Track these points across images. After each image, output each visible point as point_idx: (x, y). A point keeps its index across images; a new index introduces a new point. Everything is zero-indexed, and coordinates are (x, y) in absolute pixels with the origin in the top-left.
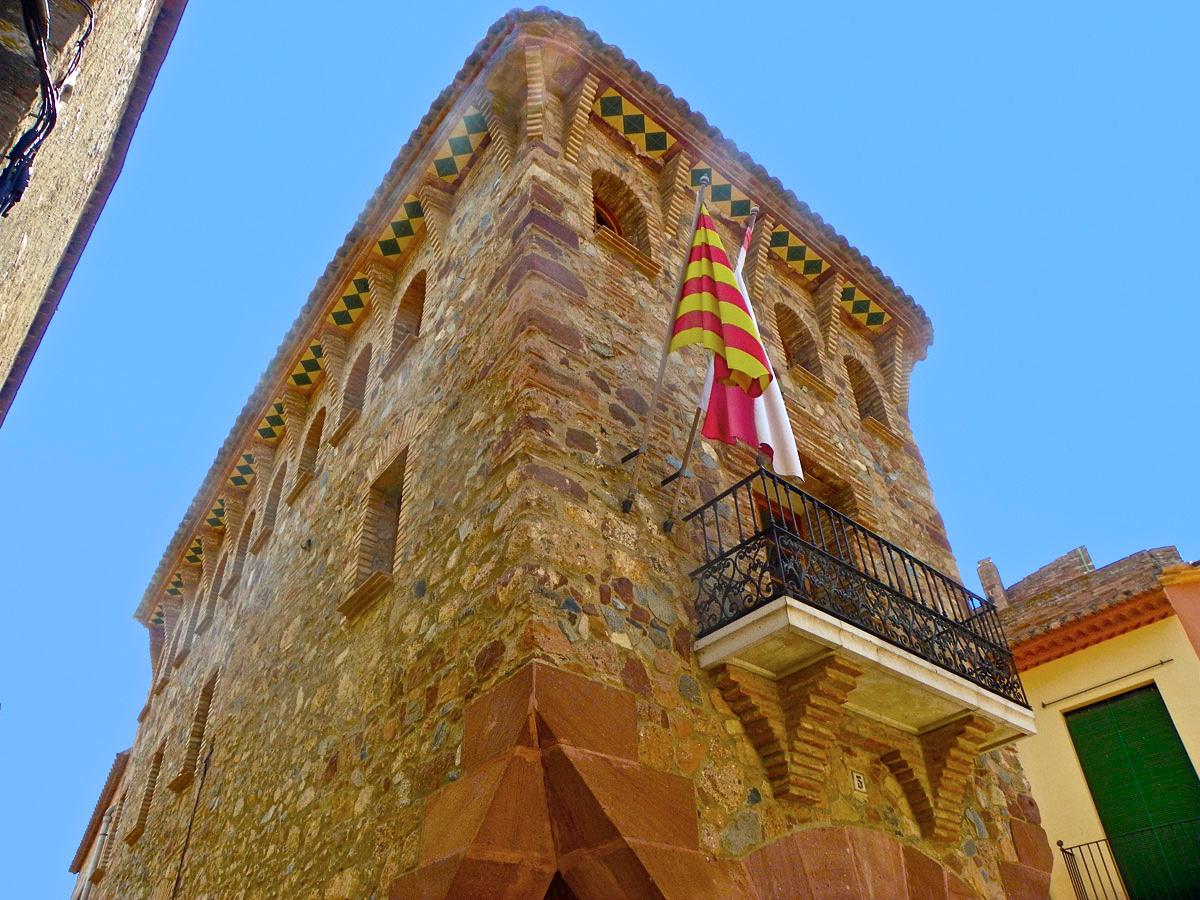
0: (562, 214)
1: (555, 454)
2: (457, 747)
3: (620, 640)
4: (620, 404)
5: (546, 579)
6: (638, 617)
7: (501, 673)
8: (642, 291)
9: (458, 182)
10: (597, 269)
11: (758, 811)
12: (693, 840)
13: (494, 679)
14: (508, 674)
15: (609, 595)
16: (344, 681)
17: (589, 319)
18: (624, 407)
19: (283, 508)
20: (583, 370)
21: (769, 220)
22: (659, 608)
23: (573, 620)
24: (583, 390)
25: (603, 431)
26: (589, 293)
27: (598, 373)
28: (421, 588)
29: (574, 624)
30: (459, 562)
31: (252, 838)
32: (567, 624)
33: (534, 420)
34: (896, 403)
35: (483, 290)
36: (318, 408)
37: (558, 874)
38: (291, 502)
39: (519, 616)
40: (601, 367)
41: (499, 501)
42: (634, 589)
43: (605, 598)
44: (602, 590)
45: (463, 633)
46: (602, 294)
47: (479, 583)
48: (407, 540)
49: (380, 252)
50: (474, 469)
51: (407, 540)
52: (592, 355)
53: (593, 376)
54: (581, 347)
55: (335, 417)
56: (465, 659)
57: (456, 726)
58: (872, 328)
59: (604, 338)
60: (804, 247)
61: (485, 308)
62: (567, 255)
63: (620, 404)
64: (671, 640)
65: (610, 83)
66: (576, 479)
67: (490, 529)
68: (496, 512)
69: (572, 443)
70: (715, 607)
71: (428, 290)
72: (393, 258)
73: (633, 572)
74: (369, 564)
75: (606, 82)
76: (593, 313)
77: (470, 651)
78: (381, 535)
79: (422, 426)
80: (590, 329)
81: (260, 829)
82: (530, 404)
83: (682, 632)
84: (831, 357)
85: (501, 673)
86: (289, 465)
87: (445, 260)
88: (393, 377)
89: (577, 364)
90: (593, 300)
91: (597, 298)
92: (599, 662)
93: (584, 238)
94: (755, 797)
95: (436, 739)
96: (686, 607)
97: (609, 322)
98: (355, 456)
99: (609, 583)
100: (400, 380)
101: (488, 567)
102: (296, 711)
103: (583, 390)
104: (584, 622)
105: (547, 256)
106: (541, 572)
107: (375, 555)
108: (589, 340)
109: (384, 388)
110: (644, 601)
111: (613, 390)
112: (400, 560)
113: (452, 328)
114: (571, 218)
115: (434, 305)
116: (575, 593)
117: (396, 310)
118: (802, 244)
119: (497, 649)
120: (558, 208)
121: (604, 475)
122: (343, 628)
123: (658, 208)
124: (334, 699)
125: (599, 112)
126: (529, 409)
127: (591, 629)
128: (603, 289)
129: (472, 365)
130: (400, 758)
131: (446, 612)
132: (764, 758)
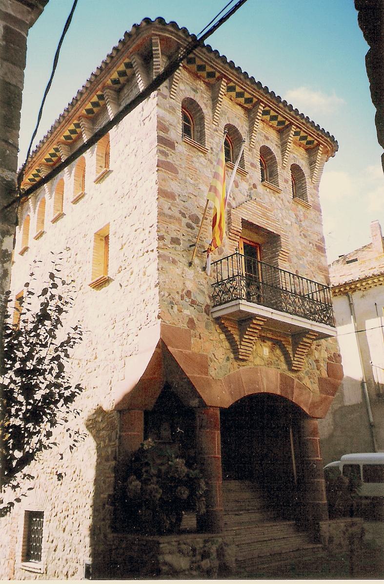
3: (187, 312)
17: (179, 185)
18: (191, 223)
76: (181, 181)
84: (283, 168)
89: (175, 208)
94: (228, 359)
110: (195, 297)
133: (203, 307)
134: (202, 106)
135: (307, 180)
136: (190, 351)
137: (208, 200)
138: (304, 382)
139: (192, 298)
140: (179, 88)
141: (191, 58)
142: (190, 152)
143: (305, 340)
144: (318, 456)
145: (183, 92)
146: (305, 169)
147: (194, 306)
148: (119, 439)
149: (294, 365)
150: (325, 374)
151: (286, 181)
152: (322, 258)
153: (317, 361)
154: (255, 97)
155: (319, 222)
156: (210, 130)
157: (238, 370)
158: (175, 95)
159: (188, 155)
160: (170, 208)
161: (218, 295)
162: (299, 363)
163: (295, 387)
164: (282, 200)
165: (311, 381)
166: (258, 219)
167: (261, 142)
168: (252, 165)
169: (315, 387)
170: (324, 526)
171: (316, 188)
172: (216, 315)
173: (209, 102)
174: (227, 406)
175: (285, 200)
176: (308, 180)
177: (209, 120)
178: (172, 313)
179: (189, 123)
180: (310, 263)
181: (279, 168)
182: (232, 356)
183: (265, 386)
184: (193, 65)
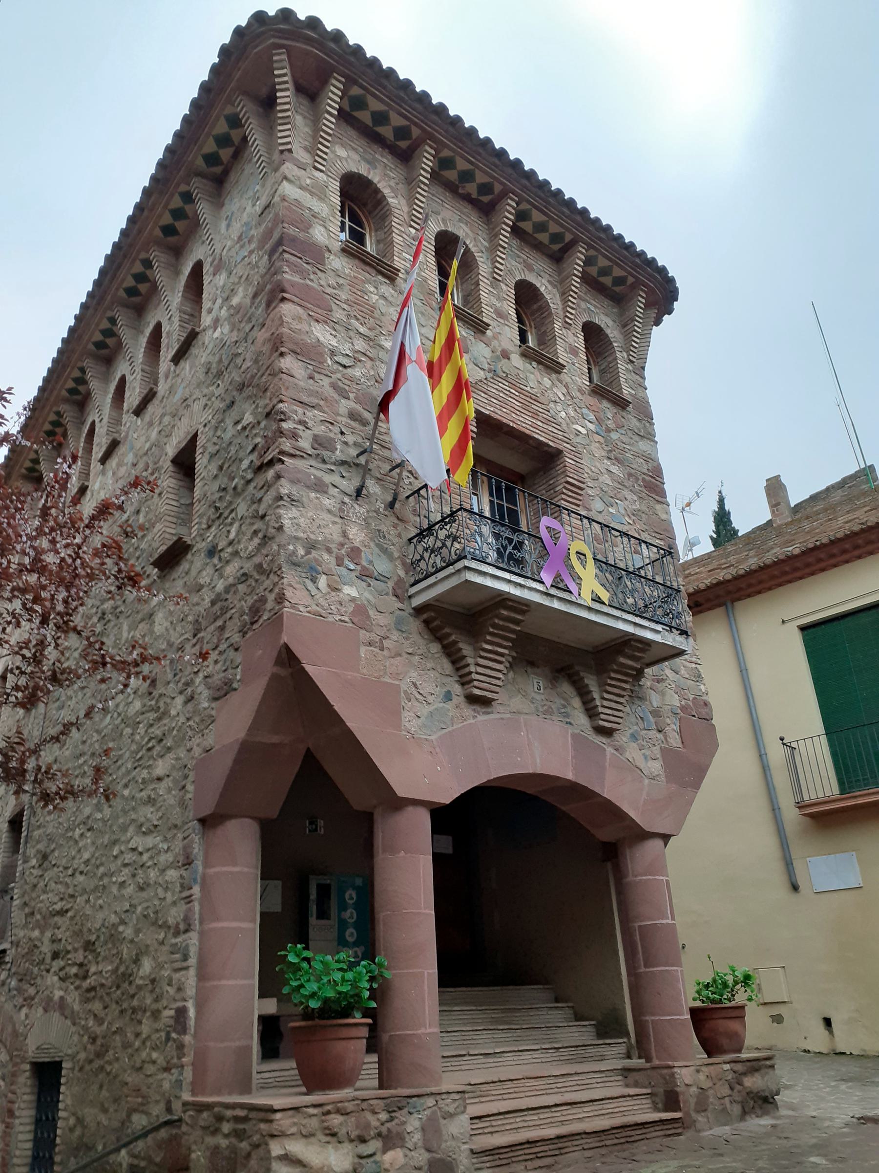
0: (310, 231)
1: (302, 456)
2: (238, 667)
3: (350, 591)
4: (359, 408)
5: (294, 553)
6: (365, 575)
7: (265, 617)
8: (384, 297)
9: (226, 173)
10: (341, 281)
11: (449, 706)
12: (398, 727)
13: (261, 621)
14: (269, 619)
15: (342, 560)
16: (159, 617)
17: (334, 333)
18: (360, 409)
19: (96, 466)
20: (326, 382)
21: (512, 199)
22: (382, 566)
23: (314, 580)
24: (325, 399)
25: (342, 433)
26: (334, 307)
27: (340, 383)
28: (212, 552)
29: (315, 583)
30: (237, 535)
31: (95, 739)
32: (309, 583)
33: (286, 430)
34: (632, 362)
35: (248, 301)
36: (118, 376)
37: (308, 749)
38: (104, 460)
39: (276, 579)
40: (343, 376)
41: (263, 491)
42: (363, 554)
43: (340, 563)
44: (337, 558)
45: (242, 588)
46: (345, 306)
47: (251, 552)
48: (200, 512)
49: (161, 235)
50: (245, 464)
51: (200, 512)
52: (336, 366)
53: (334, 386)
54: (326, 361)
55: (134, 388)
56: (242, 606)
57: (238, 654)
58: (617, 289)
59: (346, 349)
60: (548, 221)
61: (250, 318)
62: (314, 273)
63: (359, 408)
64: (391, 589)
65: (355, 82)
66: (319, 474)
67: (257, 512)
68: (260, 500)
69: (316, 446)
70: (423, 564)
71: (205, 283)
72: (172, 239)
73: (362, 542)
74: (174, 526)
75: (350, 81)
76: (337, 327)
77: (246, 602)
78: (182, 501)
79: (207, 416)
80: (334, 342)
81: (98, 732)
82: (283, 417)
83: (400, 581)
84: (567, 325)
85: (265, 617)
86: (97, 425)
87: (218, 257)
88: (182, 363)
89: (322, 377)
90: (338, 314)
91: (341, 311)
92: (332, 607)
93: (330, 251)
94: (448, 697)
95: (225, 662)
96: (404, 564)
97: (351, 333)
98: (156, 430)
99: (343, 552)
100: (188, 367)
101: (256, 541)
102: (123, 642)
103: (325, 399)
104: (323, 581)
105: (296, 279)
106: (291, 547)
107: (178, 518)
108: (333, 353)
109: (175, 371)
110: (371, 562)
111: (352, 395)
112: (196, 527)
113: (226, 329)
114: (319, 234)
115: (213, 284)
116: (316, 560)
117: (180, 294)
118: (544, 218)
119: (263, 600)
120: (307, 227)
121: (342, 469)
122: (155, 578)
123: (403, 202)
124: (152, 632)
125: (347, 108)
126: (282, 420)
127: (329, 586)
128: (346, 302)
129: (242, 369)
130: (201, 675)
131: (231, 570)
132: (458, 669)
133: (391, 584)
134: (386, 191)
135: (618, 355)
136: (356, 674)
137: (783, 622)
138: (628, 755)
139: (364, 563)
140: (334, 152)
141: (404, 138)
142: (359, 273)
143: (622, 660)
144: (668, 919)
145: (345, 163)
146: (612, 332)
147: (368, 580)
148: (638, 1048)
149: (602, 716)
150: (675, 741)
151: (574, 351)
152: (658, 507)
153: (656, 713)
154: (416, 124)
155: (649, 436)
156: (405, 236)
157: (472, 721)
158: (325, 163)
159: (355, 277)
160: (311, 377)
161: (422, 557)
162: (616, 713)
163: (607, 764)
164: (566, 386)
165: (644, 754)
166: (514, 415)
167: (517, 273)
168: (500, 314)
169: (656, 767)
170: (684, 1071)
171: (639, 372)
172: (417, 602)
173: (401, 185)
174: (446, 798)
175: (571, 386)
176: (621, 356)
177: (401, 218)
178: (314, 591)
179: (360, 225)
180: (633, 515)
181: (557, 325)
182: (457, 689)
183: (538, 761)
184: (387, 127)
